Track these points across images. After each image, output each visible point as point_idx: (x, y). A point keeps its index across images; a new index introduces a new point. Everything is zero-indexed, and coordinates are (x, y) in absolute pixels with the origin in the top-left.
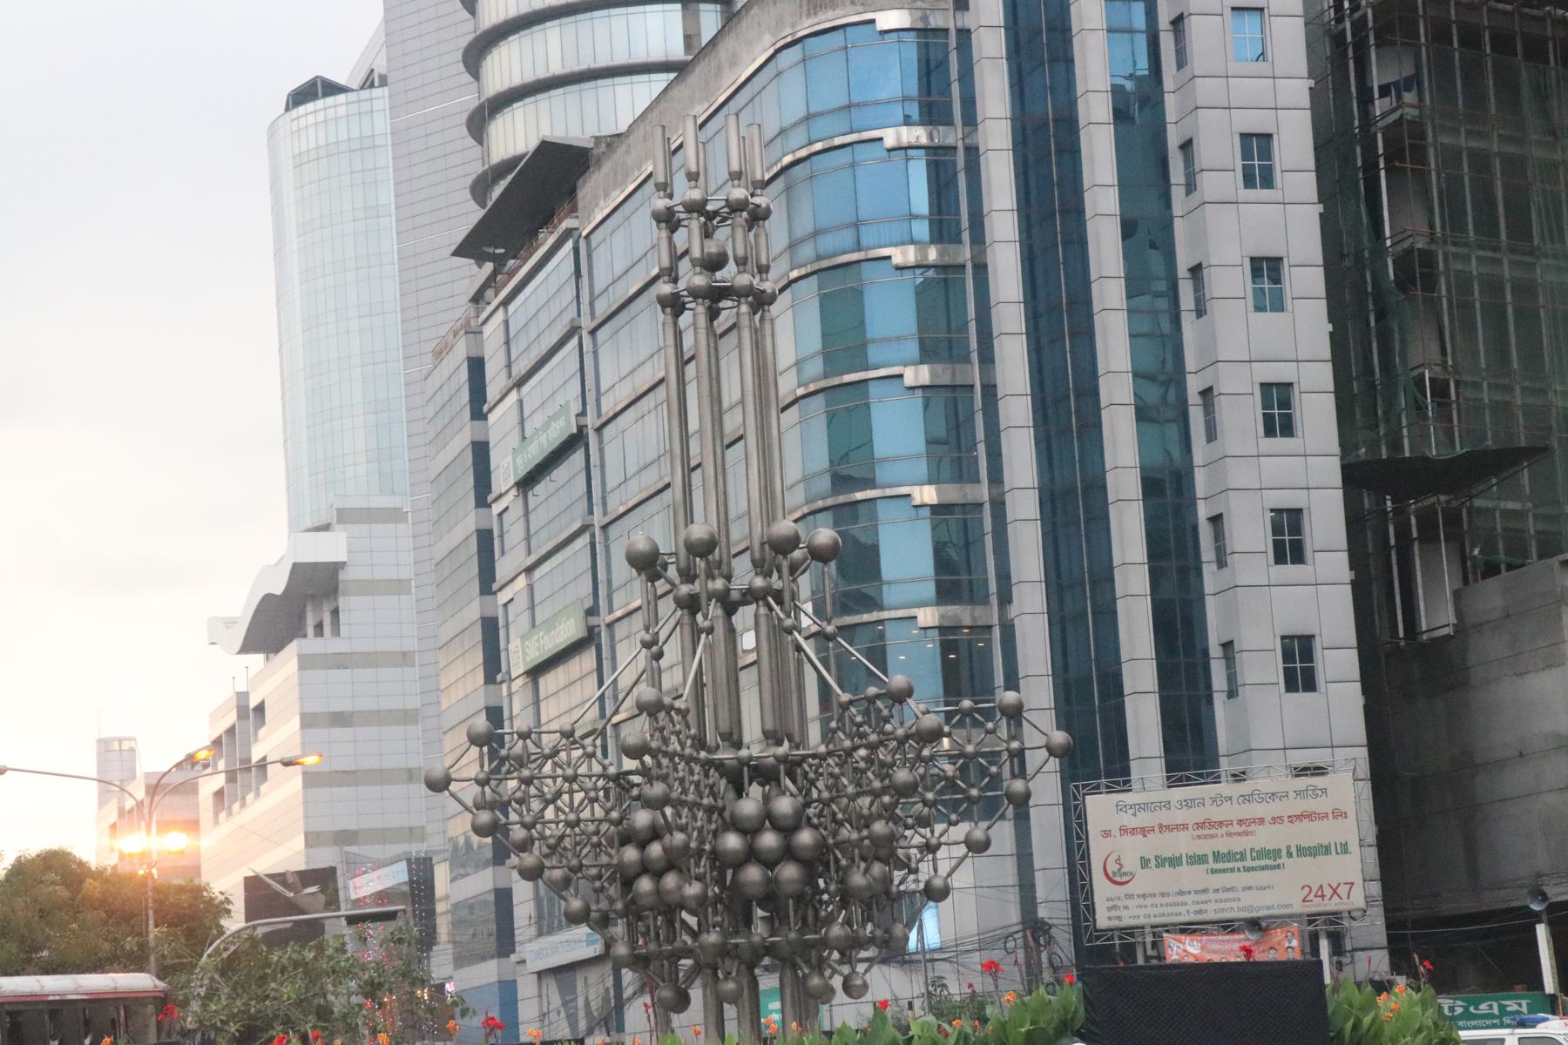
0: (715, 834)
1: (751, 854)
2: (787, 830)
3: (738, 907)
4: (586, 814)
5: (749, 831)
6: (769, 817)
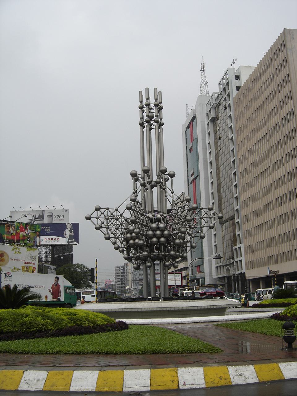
0: (147, 231)
1: (155, 236)
2: (162, 230)
3: (151, 247)
4: (179, 211)
5: (154, 230)
6: (158, 228)
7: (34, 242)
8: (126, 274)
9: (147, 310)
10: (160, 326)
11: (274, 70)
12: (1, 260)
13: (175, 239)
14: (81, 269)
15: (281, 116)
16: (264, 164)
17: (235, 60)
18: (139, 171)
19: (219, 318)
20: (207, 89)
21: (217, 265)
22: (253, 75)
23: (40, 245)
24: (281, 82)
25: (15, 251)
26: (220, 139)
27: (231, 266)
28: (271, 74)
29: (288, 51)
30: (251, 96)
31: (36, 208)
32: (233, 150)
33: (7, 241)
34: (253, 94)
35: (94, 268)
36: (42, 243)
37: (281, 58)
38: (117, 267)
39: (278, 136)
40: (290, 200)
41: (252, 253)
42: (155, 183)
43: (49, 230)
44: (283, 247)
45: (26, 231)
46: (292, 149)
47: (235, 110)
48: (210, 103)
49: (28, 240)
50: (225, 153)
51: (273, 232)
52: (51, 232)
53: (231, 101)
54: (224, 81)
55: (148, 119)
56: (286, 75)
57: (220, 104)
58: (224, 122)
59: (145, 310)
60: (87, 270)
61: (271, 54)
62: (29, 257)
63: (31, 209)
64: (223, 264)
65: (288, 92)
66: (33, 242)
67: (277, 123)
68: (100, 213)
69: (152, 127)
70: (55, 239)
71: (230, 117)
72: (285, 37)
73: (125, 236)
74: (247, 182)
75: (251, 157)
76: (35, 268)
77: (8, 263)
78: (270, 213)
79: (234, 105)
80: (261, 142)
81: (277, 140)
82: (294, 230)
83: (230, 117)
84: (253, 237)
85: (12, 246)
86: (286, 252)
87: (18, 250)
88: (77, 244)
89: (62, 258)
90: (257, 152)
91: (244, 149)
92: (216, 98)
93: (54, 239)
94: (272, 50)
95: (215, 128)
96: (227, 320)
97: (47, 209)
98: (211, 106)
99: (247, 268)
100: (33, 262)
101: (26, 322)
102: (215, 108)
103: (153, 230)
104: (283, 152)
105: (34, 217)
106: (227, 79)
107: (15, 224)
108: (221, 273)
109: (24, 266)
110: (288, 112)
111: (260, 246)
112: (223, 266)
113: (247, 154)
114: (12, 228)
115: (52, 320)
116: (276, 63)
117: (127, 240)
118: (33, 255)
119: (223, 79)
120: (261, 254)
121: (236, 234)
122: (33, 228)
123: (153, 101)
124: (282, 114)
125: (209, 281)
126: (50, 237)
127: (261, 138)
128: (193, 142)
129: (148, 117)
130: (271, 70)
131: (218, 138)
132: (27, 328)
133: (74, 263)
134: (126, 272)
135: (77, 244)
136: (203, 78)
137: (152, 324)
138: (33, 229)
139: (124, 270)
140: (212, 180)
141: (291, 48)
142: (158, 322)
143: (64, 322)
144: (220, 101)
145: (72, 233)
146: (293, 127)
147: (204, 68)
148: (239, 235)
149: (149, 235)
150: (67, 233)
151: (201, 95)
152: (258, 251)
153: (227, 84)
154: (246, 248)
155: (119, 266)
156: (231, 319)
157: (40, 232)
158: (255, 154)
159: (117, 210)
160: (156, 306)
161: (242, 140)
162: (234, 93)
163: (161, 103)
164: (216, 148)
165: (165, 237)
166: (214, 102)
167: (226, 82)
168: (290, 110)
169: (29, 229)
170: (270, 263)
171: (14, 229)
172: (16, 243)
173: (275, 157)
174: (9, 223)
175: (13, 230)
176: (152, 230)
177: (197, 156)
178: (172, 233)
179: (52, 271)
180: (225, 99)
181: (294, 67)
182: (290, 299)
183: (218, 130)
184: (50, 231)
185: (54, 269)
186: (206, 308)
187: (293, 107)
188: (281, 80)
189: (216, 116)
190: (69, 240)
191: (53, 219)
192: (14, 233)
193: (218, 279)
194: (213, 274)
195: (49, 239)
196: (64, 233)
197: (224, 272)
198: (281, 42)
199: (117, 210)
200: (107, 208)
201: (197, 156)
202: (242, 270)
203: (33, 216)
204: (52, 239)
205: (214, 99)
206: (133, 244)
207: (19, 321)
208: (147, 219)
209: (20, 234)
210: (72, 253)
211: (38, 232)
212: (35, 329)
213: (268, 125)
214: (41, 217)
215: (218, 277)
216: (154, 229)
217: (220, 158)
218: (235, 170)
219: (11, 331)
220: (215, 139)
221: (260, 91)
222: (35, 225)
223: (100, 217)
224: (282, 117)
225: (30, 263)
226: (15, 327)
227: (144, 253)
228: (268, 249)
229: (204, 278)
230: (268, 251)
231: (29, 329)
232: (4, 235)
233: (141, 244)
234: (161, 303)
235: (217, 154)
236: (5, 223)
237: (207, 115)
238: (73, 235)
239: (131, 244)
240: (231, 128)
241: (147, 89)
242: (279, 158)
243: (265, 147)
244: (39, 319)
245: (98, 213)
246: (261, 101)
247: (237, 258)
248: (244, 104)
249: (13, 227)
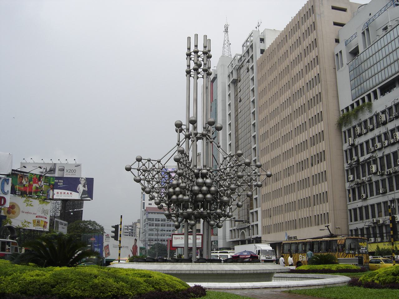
1: (201, 191)
2: (209, 186)
5: (200, 185)
6: (205, 184)
7: (48, 195)
8: (134, 233)
9: (195, 273)
10: (217, 291)
11: (301, 35)
12: (12, 212)
13: (222, 196)
14: (92, 226)
15: (306, 81)
16: (286, 128)
17: (260, 23)
19: (281, 284)
20: (229, 50)
21: (231, 229)
22: (279, 39)
23: (53, 199)
24: (307, 47)
25: (27, 203)
26: (240, 101)
27: (246, 230)
28: (298, 38)
29: (317, 16)
30: (275, 59)
31: (47, 161)
32: (254, 113)
33: (19, 193)
34: (278, 57)
35: (118, 225)
36: (55, 197)
37: (309, 22)
38: (126, 226)
39: (302, 100)
40: (312, 165)
41: (269, 218)
42: (201, 135)
43: (62, 184)
44: (305, 212)
45: (40, 183)
46: (316, 114)
47: (258, 73)
48: (232, 65)
49: (40, 193)
50: (245, 115)
51: (292, 197)
52: (64, 186)
53: (254, 64)
54: (248, 44)
55: (196, 67)
56: (313, 40)
57: (242, 66)
58: (245, 85)
59: (194, 273)
60: (98, 227)
61: (298, 18)
62: (41, 211)
63: (42, 162)
64: (237, 227)
65: (314, 57)
66: (46, 195)
67: (301, 87)
68: (141, 164)
69: (199, 76)
70: (68, 193)
71: (253, 79)
72: (314, 2)
73: (167, 190)
74: (267, 146)
75: (273, 120)
76: (47, 223)
77: (19, 216)
78: (291, 177)
79: (258, 67)
80: (284, 106)
81: (301, 104)
82: (314, 195)
83: (253, 79)
84: (271, 201)
85: (24, 198)
86: (305, 218)
87: (30, 203)
88: (90, 200)
89: (72, 214)
90: (279, 116)
91: (266, 112)
92: (238, 60)
93: (66, 193)
94: (299, 15)
95: (236, 90)
96: (289, 286)
97: (59, 162)
98: (233, 67)
99: (263, 233)
100: (45, 216)
101: (96, 284)
102: (237, 70)
103: (198, 185)
104: (307, 117)
105: (45, 170)
106: (252, 41)
107: (29, 175)
108: (235, 237)
109: (35, 220)
110: (313, 77)
111: (278, 210)
112: (238, 230)
113: (269, 117)
114: (25, 179)
115: (127, 282)
116: (304, 28)
117: (169, 195)
118: (45, 209)
119: (247, 41)
120: (279, 219)
121: (252, 198)
122: (48, 181)
123: (201, 48)
124: (307, 78)
125: (222, 244)
126: (63, 191)
127: (284, 102)
128: (213, 103)
129: (196, 65)
130: (298, 34)
131: (239, 100)
132: (101, 292)
133: (83, 219)
134: (134, 231)
135: (90, 200)
136: (226, 39)
137: (209, 289)
138: (47, 182)
139: (132, 230)
140: (231, 142)
141: (319, 13)
142: (215, 287)
143: (142, 285)
144: (242, 63)
145: (86, 188)
146: (318, 92)
147: (227, 29)
148: (256, 199)
149: (195, 190)
150: (81, 188)
151: (223, 56)
152: (276, 215)
153: (252, 46)
154: (263, 212)
155: (127, 225)
156: (293, 285)
157: (53, 185)
158: (277, 117)
159: (159, 162)
160: (205, 269)
161: (264, 103)
162: (258, 55)
163: (210, 51)
164: (236, 110)
165: (212, 194)
166: (236, 63)
167: (250, 44)
168: (316, 75)
169: (42, 181)
170: (288, 228)
171: (27, 180)
172: (29, 195)
173: (298, 121)
174: (23, 174)
175: (26, 181)
176: (198, 186)
177: (216, 117)
178: (219, 190)
179: (63, 226)
180: (248, 62)
181: (321, 32)
182: (331, 265)
183: (239, 92)
184: (63, 184)
185: (65, 225)
186: (259, 272)
187: (319, 72)
188: (308, 45)
189: (238, 77)
190: (82, 196)
191: (65, 173)
192: (27, 185)
193: (231, 243)
194: (227, 238)
195: (61, 193)
196: (78, 188)
197: (238, 236)
198: (310, 7)
199: (159, 162)
200: (149, 159)
201: (216, 117)
202: (258, 234)
203: (44, 169)
204: (64, 193)
205: (237, 61)
206: (176, 200)
207: (88, 282)
208: (192, 173)
209: (33, 185)
210: (82, 209)
211: (51, 185)
212: (110, 293)
213: (292, 89)
214: (52, 170)
215: (232, 240)
216: (200, 184)
217: (239, 121)
218: (255, 133)
219: (81, 296)
220: (236, 100)
221: (286, 54)
222: (49, 178)
224: (307, 82)
225: (42, 217)
226: (84, 290)
227: (188, 210)
228: (286, 214)
229: (217, 241)
230: (286, 216)
231: (103, 293)
232: (16, 185)
233: (186, 199)
234: (210, 266)
235: (236, 116)
236: (18, 173)
237: (229, 76)
238: (87, 190)
239: (174, 199)
240: (253, 90)
241: (196, 36)
242: (302, 122)
243: (289, 111)
244: (111, 280)
245: (139, 164)
246: (286, 65)
247: (253, 222)
248: (268, 67)
249: (26, 178)
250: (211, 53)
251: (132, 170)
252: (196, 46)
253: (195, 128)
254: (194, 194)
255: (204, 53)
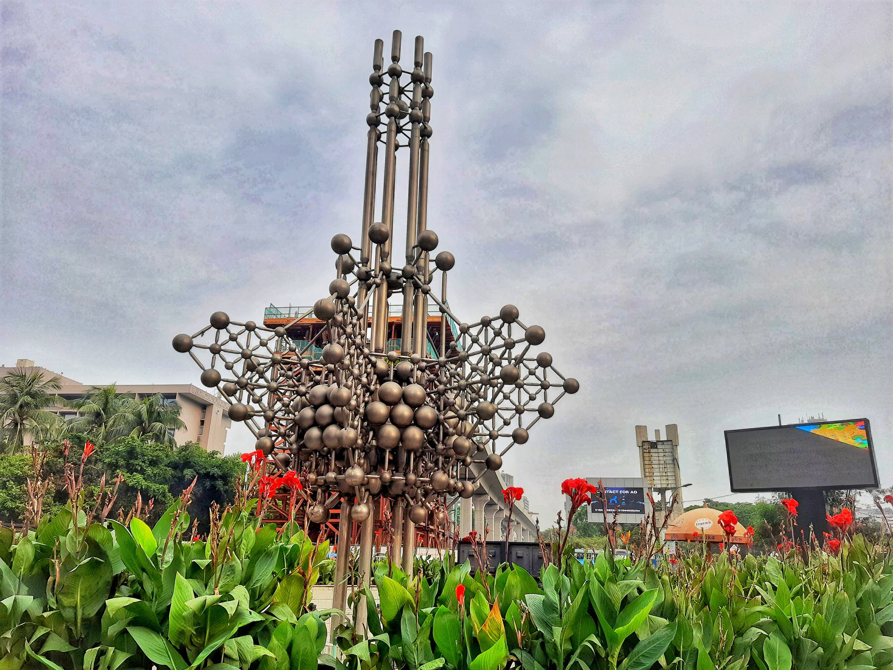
2: (415, 406)
6: (404, 398)
18: (356, 237)
68: (224, 335)
69: (402, 139)
117: (300, 428)
123: (407, 63)
165: (423, 428)
223: (223, 347)
241: (397, 35)
250: (431, 124)
251: (194, 350)
252: (395, 59)
253: (384, 256)
254: (372, 425)
255: (416, 79)
